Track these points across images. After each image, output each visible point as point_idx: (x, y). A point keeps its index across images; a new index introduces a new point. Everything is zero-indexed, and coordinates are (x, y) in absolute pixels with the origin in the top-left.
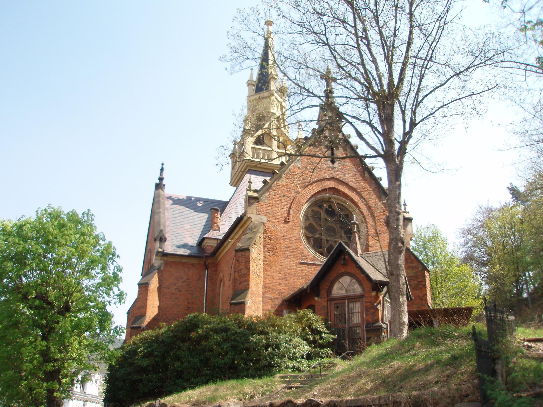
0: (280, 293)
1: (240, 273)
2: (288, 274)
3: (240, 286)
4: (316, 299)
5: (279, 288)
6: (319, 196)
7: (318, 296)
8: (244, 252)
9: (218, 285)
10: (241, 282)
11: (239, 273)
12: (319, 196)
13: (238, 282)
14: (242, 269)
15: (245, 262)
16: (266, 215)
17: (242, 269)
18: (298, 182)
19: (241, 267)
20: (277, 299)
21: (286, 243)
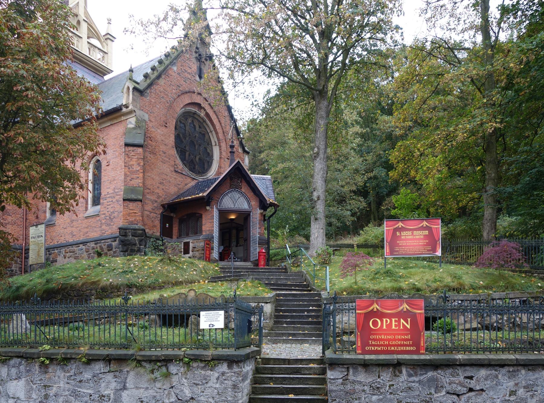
0: (159, 197)
1: (131, 169)
4: (208, 208)
6: (189, 108)
8: (135, 148)
10: (132, 179)
11: (129, 169)
12: (189, 108)
13: (129, 178)
14: (133, 165)
15: (137, 158)
16: (147, 113)
17: (133, 165)
18: (174, 87)
19: (131, 163)
20: (156, 202)
21: (163, 148)
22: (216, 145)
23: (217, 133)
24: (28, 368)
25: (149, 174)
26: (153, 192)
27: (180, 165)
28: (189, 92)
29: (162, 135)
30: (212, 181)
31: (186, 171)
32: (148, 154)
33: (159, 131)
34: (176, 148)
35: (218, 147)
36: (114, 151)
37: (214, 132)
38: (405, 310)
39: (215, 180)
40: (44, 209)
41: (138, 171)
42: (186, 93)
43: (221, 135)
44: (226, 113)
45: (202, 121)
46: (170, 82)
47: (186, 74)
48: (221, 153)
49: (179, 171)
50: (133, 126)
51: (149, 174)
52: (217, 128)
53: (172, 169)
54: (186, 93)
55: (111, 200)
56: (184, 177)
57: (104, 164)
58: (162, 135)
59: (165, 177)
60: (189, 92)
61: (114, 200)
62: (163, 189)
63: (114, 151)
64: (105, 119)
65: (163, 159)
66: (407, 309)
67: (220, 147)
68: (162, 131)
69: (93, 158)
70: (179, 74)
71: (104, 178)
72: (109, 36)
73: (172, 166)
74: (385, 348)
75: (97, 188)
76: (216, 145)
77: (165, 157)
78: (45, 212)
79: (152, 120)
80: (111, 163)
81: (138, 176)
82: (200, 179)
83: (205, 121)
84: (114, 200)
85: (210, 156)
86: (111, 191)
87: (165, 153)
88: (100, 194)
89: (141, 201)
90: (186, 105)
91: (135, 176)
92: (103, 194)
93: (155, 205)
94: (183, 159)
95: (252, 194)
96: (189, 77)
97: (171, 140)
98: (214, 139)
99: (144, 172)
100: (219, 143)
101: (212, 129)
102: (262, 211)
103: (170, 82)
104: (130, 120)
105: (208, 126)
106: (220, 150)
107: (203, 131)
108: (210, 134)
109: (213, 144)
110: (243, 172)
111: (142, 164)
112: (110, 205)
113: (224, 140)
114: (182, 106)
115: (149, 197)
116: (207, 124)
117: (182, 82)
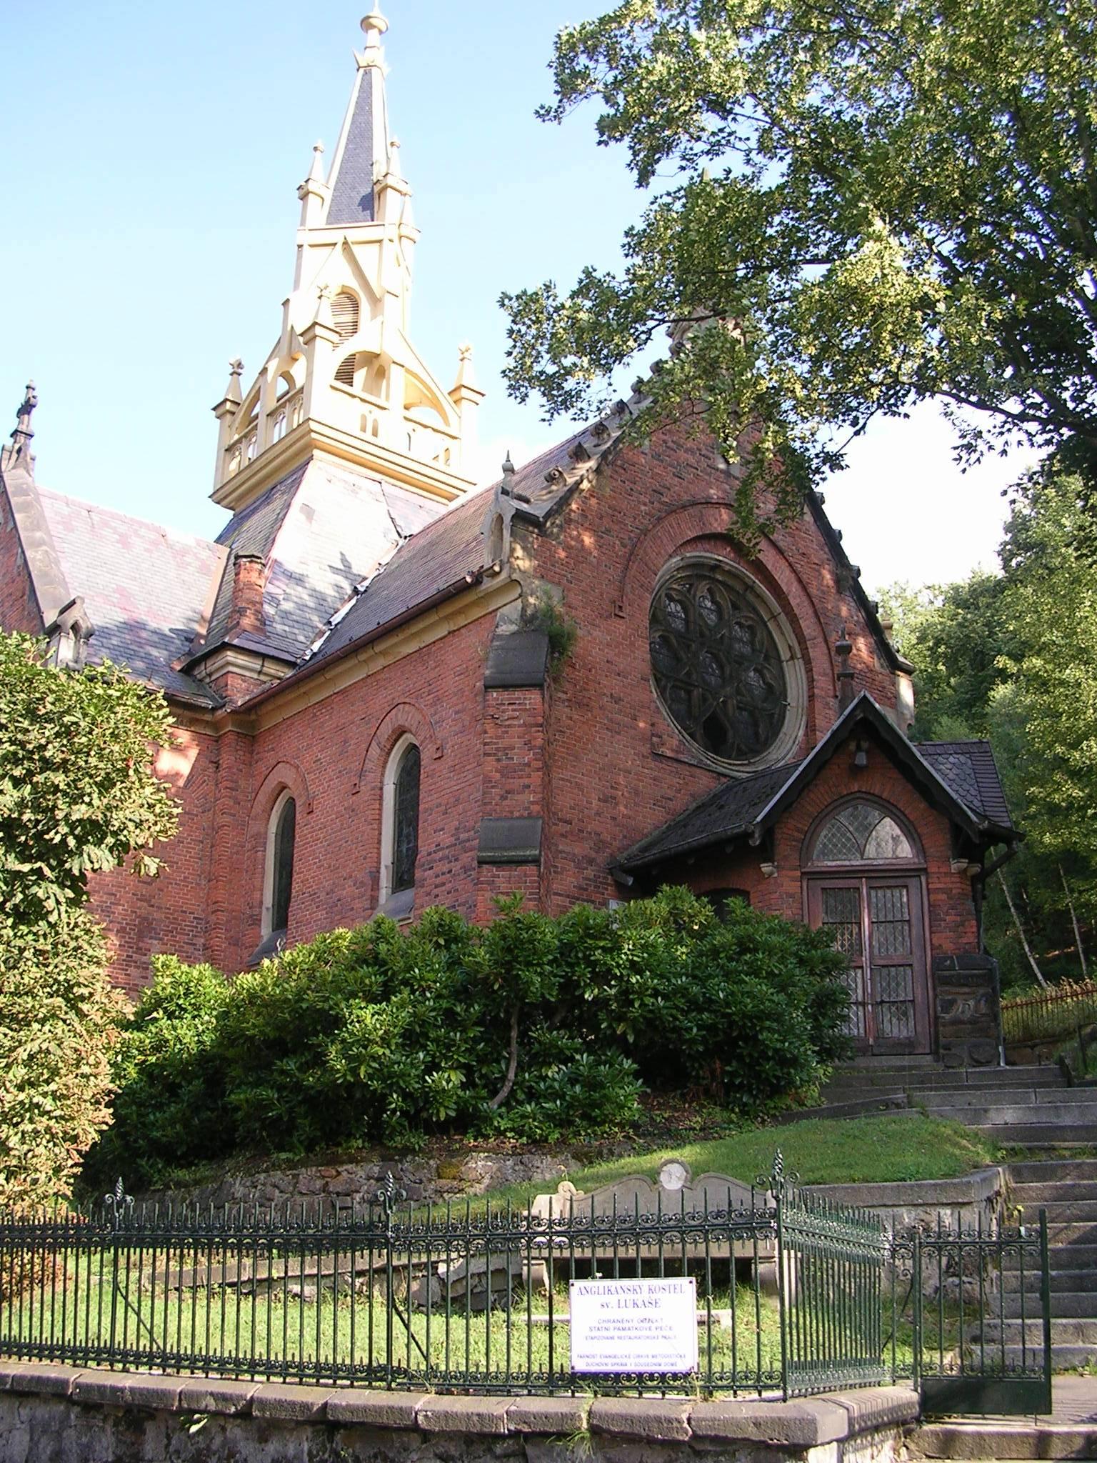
0: (600, 845)
3: (505, 803)
4: (766, 868)
5: (593, 826)
7: (770, 859)
9: (258, 808)
15: (525, 725)
16: (559, 584)
19: (505, 742)
20: (591, 861)
22: (792, 658)
23: (794, 620)
24: (84, 1440)
25: (566, 774)
26: (581, 831)
27: (673, 736)
28: (694, 504)
29: (608, 645)
30: (772, 778)
31: (695, 750)
32: (563, 711)
33: (596, 633)
34: (657, 680)
35: (800, 664)
36: (457, 713)
37: (783, 618)
39: (789, 769)
40: (256, 911)
41: (528, 765)
42: (684, 507)
43: (808, 626)
44: (824, 555)
45: (739, 588)
46: (628, 485)
47: (681, 453)
48: (811, 681)
49: (669, 754)
50: (514, 628)
51: (566, 774)
52: (793, 602)
53: (645, 750)
54: (684, 507)
55: (445, 870)
56: (685, 771)
57: (426, 756)
58: (608, 645)
60: (694, 504)
61: (456, 867)
62: (614, 819)
63: (457, 713)
64: (433, 618)
65: (611, 720)
67: (808, 661)
69: (396, 740)
70: (657, 456)
71: (427, 799)
72: (464, 392)
74: (787, 1321)
75: (408, 836)
76: (792, 658)
78: (257, 921)
79: (575, 603)
80: (448, 751)
81: (526, 781)
82: (742, 771)
83: (750, 588)
84: (456, 867)
85: (776, 694)
86: (445, 838)
87: (617, 701)
88: (414, 851)
89: (536, 861)
90: (685, 543)
91: (517, 783)
92: (423, 850)
93: (590, 872)
94: (683, 718)
95: (923, 805)
96: (692, 460)
97: (639, 658)
98: (784, 642)
99: (547, 769)
100: (805, 651)
101: (777, 608)
102: (964, 863)
103: (628, 485)
104: (505, 610)
105: (764, 602)
106: (809, 671)
107: (747, 618)
108: (771, 625)
109: (785, 654)
110: (884, 734)
111: (539, 742)
112: (444, 884)
113: (820, 640)
114: (671, 549)
115: (568, 849)
116: (758, 596)
117: (670, 480)
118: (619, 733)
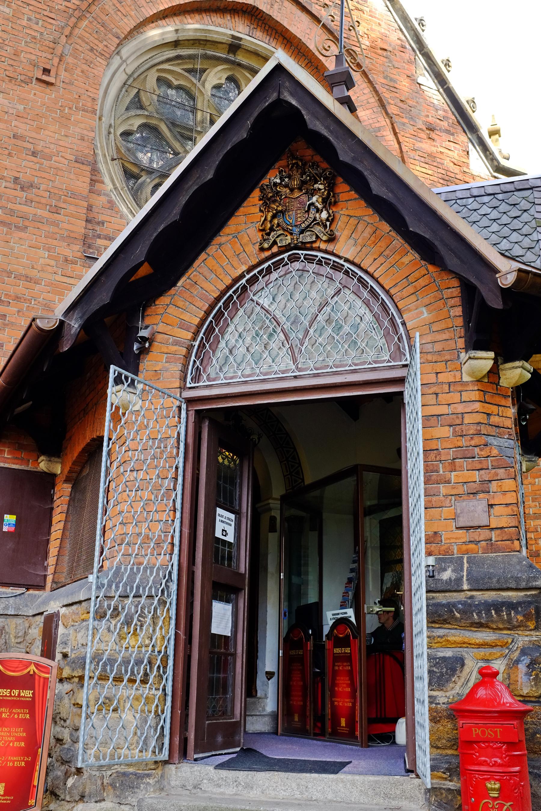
2: (17, 298)
38: (32, 673)
59: (21, 288)
65: (12, 212)
66: (34, 671)
68: (21, 100)
73: (70, 239)
77: (29, 202)
118: (24, 229)
